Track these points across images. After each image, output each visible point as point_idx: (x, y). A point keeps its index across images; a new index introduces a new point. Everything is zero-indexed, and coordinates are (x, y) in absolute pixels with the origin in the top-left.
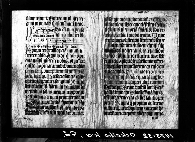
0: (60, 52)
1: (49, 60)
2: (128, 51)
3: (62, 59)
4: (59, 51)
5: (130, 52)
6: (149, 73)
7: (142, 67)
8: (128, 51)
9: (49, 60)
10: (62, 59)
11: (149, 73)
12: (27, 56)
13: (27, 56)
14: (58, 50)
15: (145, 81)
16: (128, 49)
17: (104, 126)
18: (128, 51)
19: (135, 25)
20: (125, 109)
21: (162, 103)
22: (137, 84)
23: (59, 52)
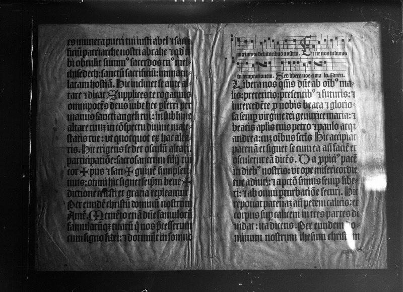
0: (293, 130)
1: (324, 178)
2: (132, 52)
3: (172, 112)
4: (292, 128)
5: (123, 76)
6: (117, 208)
7: (128, 42)
8: (132, 52)
9: (324, 178)
10: (172, 112)
11: (117, 208)
12: (325, 182)
13: (325, 182)
14: (289, 126)
15: (136, 93)
16: (133, 48)
17: (212, 267)
18: (113, 106)
19: (118, 139)
20: (136, 130)
21: (126, 51)
22: (334, 228)
23: (291, 131)
